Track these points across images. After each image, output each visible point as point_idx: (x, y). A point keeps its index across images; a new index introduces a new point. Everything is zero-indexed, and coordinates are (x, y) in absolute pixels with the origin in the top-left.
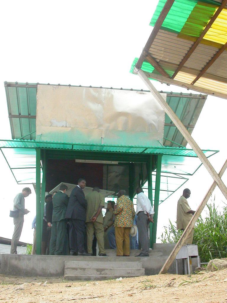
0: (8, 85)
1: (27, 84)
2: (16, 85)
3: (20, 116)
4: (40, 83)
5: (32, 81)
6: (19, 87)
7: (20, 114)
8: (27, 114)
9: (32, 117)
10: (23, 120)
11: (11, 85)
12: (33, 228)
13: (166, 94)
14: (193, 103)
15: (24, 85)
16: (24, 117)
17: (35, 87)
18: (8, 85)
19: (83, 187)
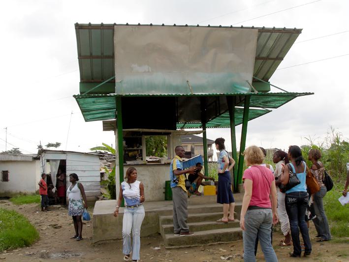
0: (79, 27)
1: (102, 25)
2: (90, 27)
3: (91, 57)
4: (117, 23)
5: (107, 22)
6: (93, 29)
7: (91, 54)
8: (100, 54)
9: (82, 28)
10: (95, 60)
11: (265, 62)
12: (103, 144)
13: (257, 30)
14: (286, 37)
15: (86, 26)
16: (97, 57)
17: (112, 28)
18: (79, 27)
19: (193, 168)
